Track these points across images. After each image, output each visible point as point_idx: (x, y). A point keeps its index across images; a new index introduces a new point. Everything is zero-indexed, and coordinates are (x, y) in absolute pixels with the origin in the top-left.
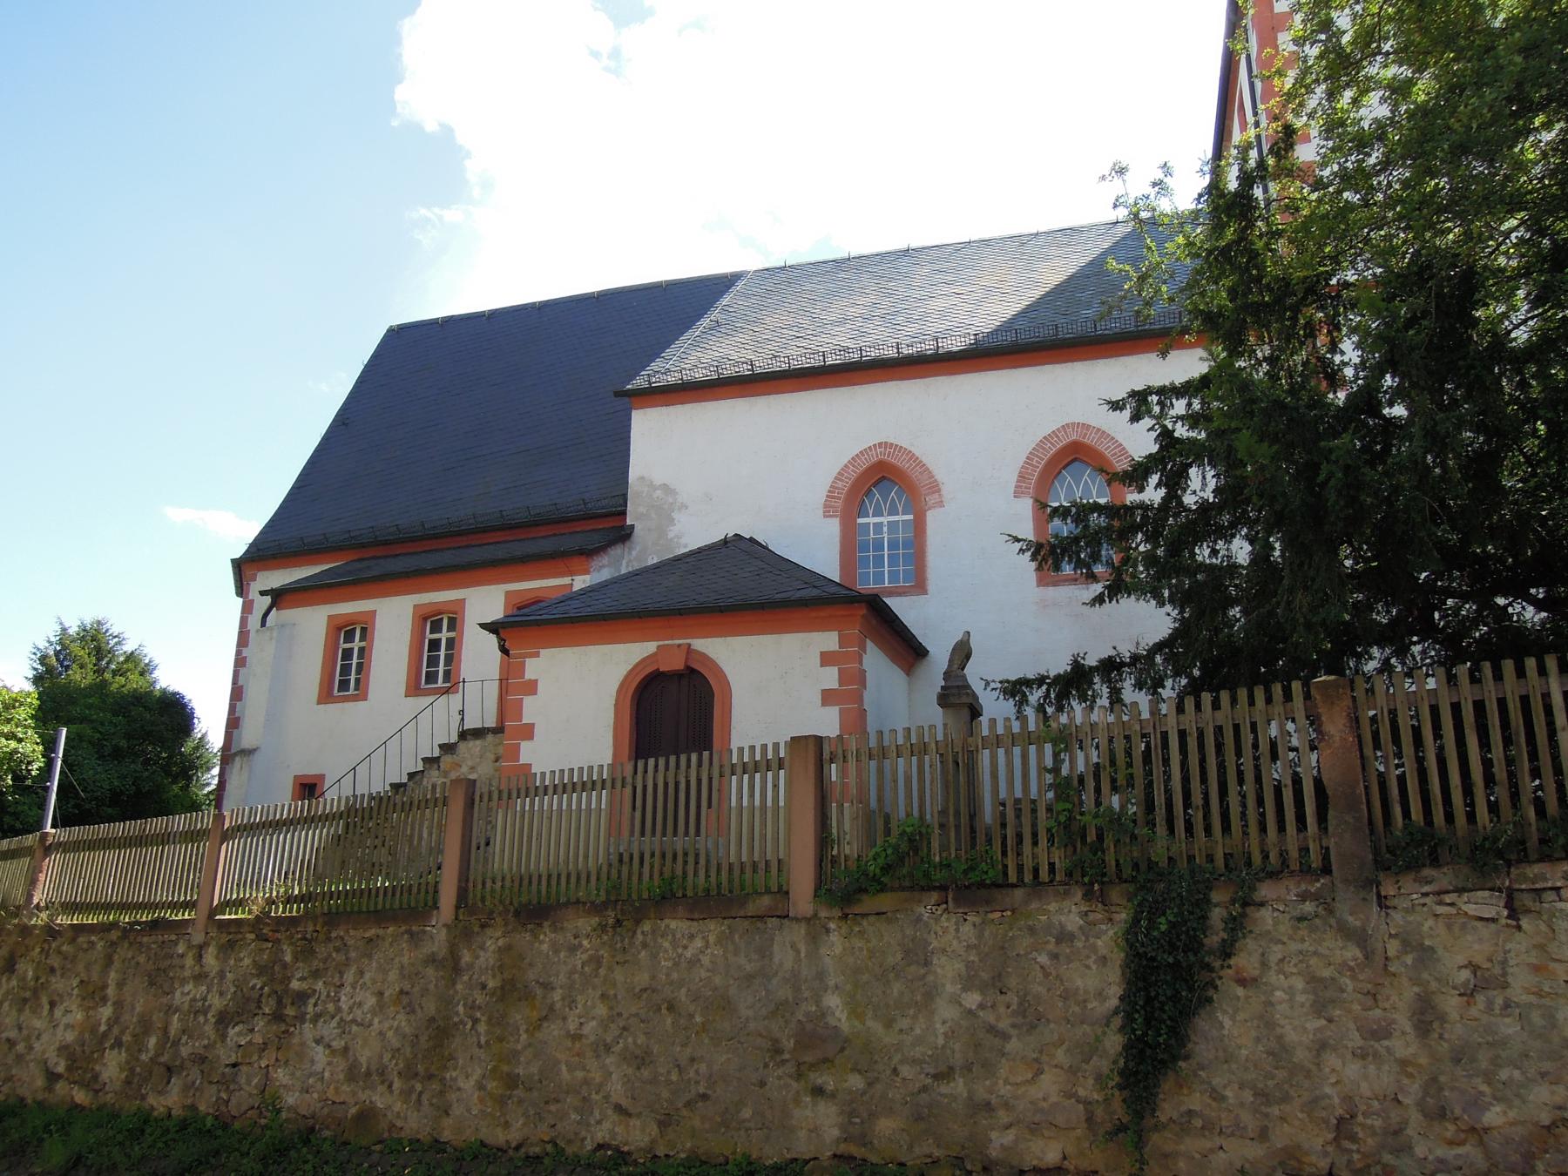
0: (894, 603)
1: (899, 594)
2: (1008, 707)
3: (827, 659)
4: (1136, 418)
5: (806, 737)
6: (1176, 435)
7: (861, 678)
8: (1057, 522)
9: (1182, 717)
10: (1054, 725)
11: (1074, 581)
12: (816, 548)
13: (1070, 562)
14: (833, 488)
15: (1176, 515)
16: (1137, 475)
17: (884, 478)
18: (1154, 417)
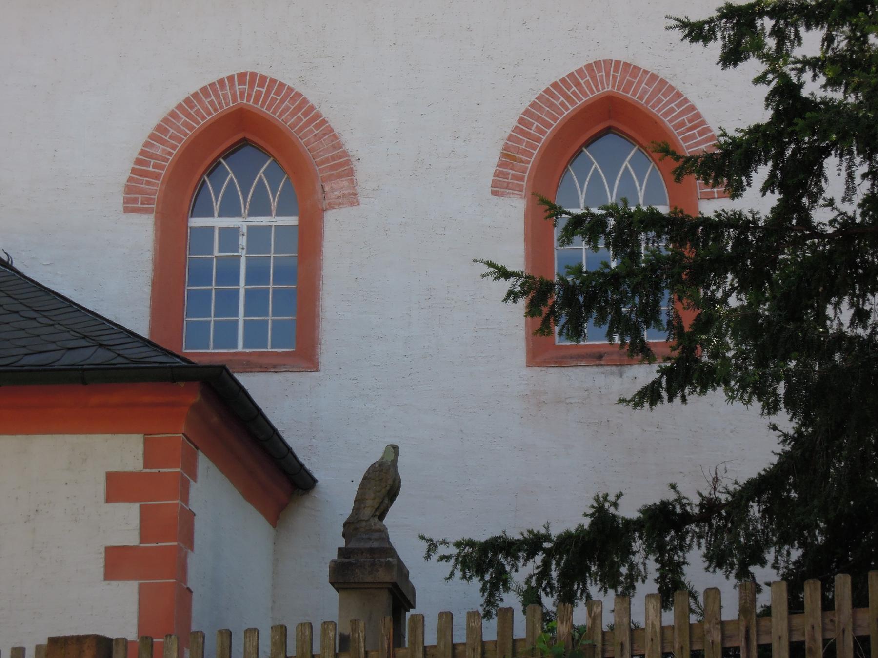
0: (258, 386)
1: (265, 368)
2: (469, 593)
3: (118, 487)
4: (732, 57)
5: (79, 640)
6: (805, 93)
7: (184, 527)
8: (580, 246)
9: (797, 620)
10: (562, 628)
11: (597, 358)
12: (109, 273)
13: (600, 321)
14: (144, 156)
15: (797, 243)
16: (729, 163)
17: (244, 143)
18: (766, 57)
